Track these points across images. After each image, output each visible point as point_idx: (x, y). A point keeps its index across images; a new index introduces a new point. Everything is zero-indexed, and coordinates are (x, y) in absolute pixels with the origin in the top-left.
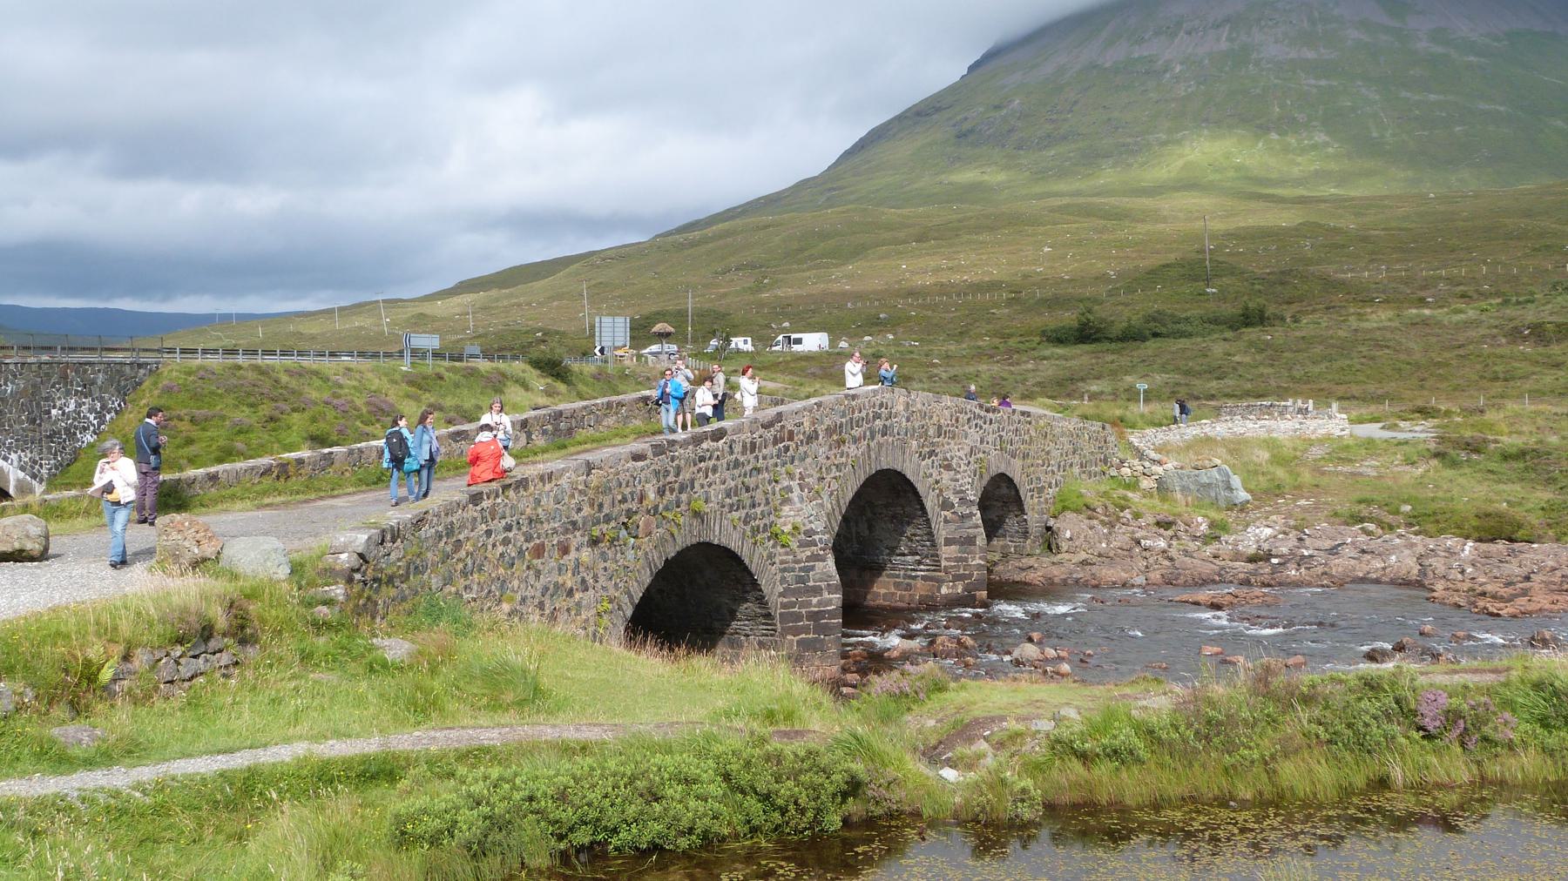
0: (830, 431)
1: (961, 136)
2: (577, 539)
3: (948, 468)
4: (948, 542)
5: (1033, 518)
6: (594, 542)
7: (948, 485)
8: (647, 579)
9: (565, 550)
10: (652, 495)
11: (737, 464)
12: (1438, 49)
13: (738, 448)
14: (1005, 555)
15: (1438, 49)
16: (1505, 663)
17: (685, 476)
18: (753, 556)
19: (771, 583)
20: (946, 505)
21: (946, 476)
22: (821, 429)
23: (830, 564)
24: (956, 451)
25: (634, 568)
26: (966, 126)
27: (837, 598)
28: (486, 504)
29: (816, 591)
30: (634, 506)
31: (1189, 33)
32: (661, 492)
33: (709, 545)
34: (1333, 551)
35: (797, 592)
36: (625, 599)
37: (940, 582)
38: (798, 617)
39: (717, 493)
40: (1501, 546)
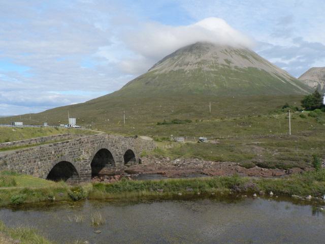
0: (91, 142)
1: (147, 83)
2: (38, 160)
3: (117, 148)
4: (117, 162)
5: (136, 157)
6: (41, 160)
7: (117, 153)
8: (52, 167)
9: (35, 162)
10: (53, 153)
11: (71, 147)
12: (236, 70)
13: (71, 144)
14: (132, 164)
15: (236, 70)
16: (22, 144)
17: (60, 149)
18: (75, 164)
19: (78, 168)
20: (117, 155)
21: (117, 150)
22: (89, 141)
23: (90, 165)
24: (119, 146)
25: (49, 165)
26: (147, 82)
27: (90, 171)
28: (19, 153)
29: (86, 170)
30: (50, 154)
31: (190, 65)
32: (55, 152)
33: (65, 162)
34: (189, 164)
35: (83, 170)
36: (47, 171)
37: (116, 169)
38: (83, 175)
39: (67, 153)
40: (219, 163)
